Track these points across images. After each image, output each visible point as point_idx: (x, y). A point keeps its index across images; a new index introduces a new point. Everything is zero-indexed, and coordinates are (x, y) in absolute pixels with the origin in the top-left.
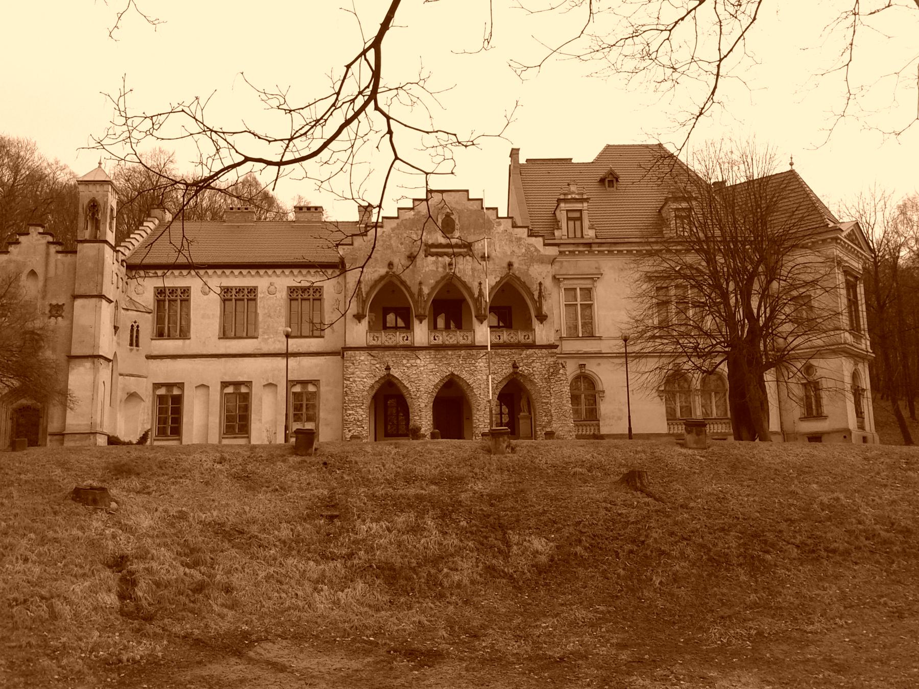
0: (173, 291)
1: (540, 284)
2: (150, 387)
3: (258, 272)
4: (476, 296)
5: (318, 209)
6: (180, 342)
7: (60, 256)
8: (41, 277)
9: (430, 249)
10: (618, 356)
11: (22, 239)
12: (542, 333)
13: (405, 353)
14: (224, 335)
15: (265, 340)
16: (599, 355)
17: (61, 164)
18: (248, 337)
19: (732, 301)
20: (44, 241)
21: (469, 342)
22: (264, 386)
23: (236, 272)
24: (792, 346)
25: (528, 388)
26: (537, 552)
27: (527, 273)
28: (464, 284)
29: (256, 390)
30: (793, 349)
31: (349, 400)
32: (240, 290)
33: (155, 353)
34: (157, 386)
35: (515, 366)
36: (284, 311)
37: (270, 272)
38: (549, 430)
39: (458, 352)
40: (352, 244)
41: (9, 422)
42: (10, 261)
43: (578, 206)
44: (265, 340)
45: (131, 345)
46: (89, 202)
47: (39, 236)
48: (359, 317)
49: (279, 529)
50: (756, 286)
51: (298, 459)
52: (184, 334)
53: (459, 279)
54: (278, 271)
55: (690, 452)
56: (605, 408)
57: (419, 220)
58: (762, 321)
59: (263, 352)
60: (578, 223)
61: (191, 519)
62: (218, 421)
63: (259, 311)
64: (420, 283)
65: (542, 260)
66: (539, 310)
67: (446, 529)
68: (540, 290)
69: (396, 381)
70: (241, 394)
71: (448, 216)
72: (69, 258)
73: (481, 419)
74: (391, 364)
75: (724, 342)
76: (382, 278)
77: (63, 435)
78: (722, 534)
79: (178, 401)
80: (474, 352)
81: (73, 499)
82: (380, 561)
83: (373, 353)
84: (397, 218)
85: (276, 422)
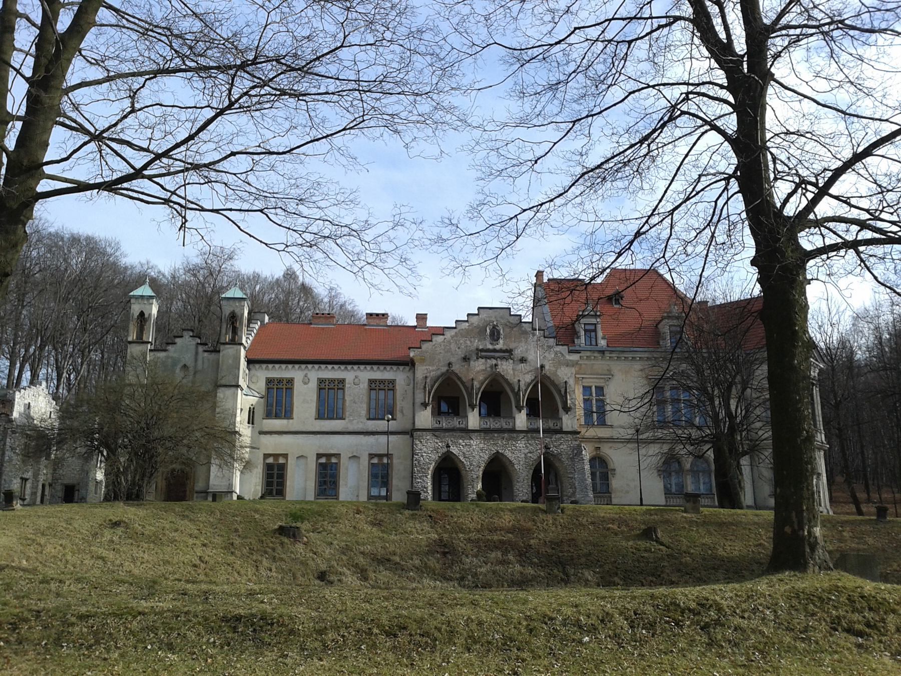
0: (280, 381)
1: (566, 382)
2: (261, 457)
3: (346, 368)
4: (516, 390)
5: (384, 316)
6: (285, 422)
7: (206, 354)
8: (191, 369)
9: (481, 353)
10: (629, 441)
11: (178, 340)
12: (568, 422)
13: (461, 434)
14: (320, 416)
15: (351, 421)
16: (610, 440)
17: (151, 265)
18: (337, 419)
19: (717, 402)
20: (194, 343)
21: (510, 427)
22: (350, 458)
23: (330, 367)
24: (763, 437)
25: (557, 465)
26: (588, 580)
27: (555, 374)
28: (506, 381)
29: (344, 461)
30: (765, 439)
31: (418, 470)
32: (332, 381)
33: (266, 429)
34: (266, 456)
35: (547, 447)
36: (365, 399)
37: (356, 367)
38: (573, 499)
39: (502, 435)
40: (420, 348)
41: (164, 481)
42: (167, 357)
43: (593, 321)
44: (351, 421)
45: (249, 423)
46: (230, 314)
47: (191, 339)
48: (425, 405)
49: (412, 559)
50: (734, 391)
51: (411, 512)
52: (288, 415)
53: (503, 377)
54: (362, 367)
55: (689, 515)
56: (615, 483)
57: (472, 330)
58: (738, 420)
59: (348, 430)
60: (593, 334)
61: (354, 550)
62: (314, 485)
63: (346, 398)
64: (473, 379)
65: (568, 364)
66: (565, 402)
67: (523, 564)
68: (566, 387)
69: (453, 457)
70: (383, 464)
71: (494, 327)
72: (213, 356)
73: (521, 489)
74: (450, 443)
75: (711, 435)
76: (442, 374)
77: (207, 493)
78: (713, 571)
79: (282, 468)
80: (515, 435)
81: (280, 534)
82: (483, 583)
83: (436, 433)
84: (455, 328)
85: (358, 487)
